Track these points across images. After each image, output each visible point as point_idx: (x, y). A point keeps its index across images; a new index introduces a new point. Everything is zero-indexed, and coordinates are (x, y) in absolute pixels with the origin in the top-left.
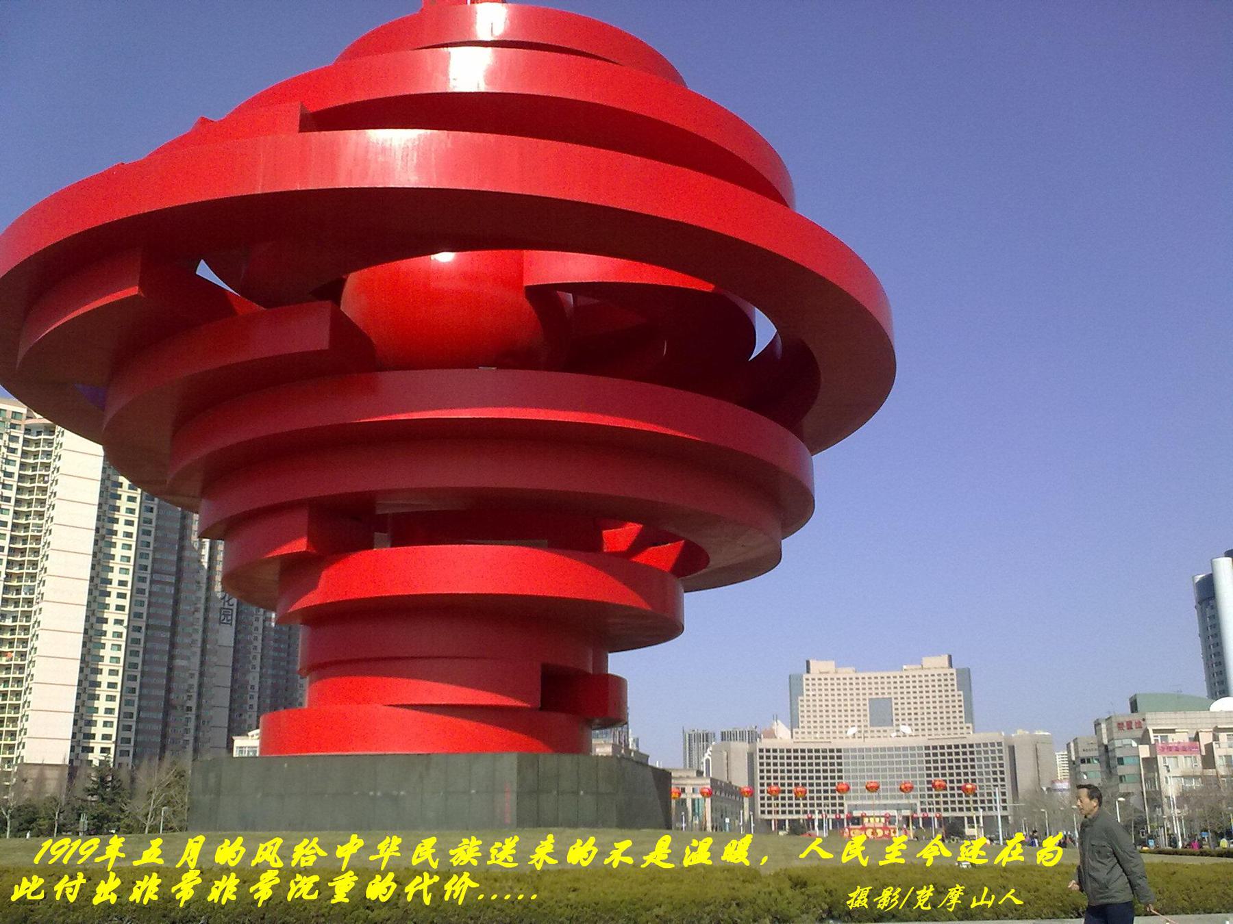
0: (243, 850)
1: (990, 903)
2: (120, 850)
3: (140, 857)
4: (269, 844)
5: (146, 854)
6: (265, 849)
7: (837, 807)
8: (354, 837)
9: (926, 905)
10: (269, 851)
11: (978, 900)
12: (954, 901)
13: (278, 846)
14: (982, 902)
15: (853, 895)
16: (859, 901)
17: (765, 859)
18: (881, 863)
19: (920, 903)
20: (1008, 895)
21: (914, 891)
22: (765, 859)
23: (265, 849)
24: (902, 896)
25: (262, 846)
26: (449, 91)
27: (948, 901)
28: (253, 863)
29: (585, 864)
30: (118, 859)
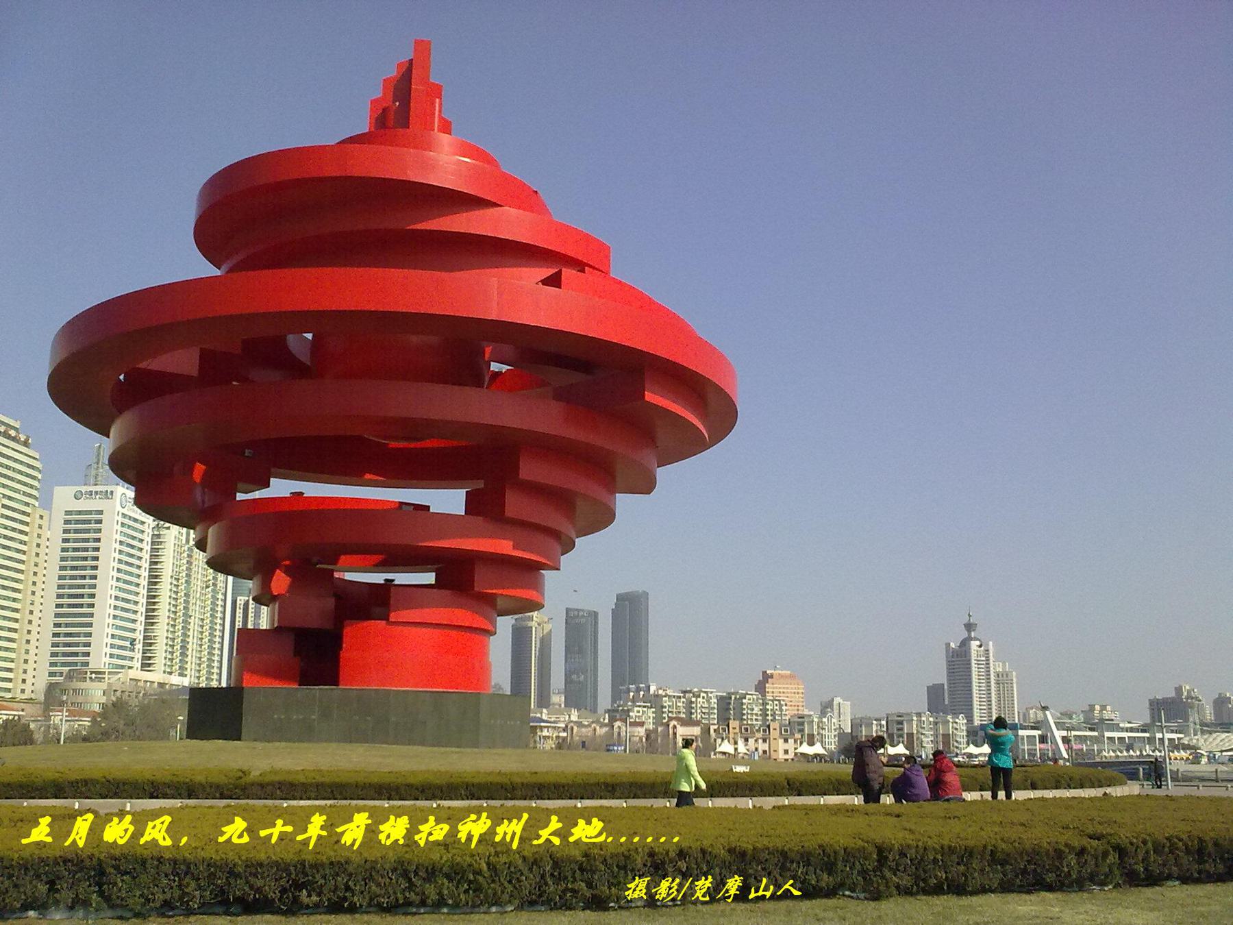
0: (132, 828)
1: (768, 894)
2: (322, 828)
3: (28, 836)
4: (158, 822)
5: (35, 832)
6: (154, 827)
7: (974, 776)
8: (238, 819)
9: (704, 896)
10: (157, 829)
11: (757, 891)
12: (732, 892)
13: (166, 824)
14: (760, 893)
15: (632, 886)
16: (637, 892)
17: (184, 840)
18: (24, 841)
19: (699, 894)
20: (787, 886)
21: (692, 882)
22: (184, 840)
23: (154, 827)
24: (681, 886)
25: (150, 824)
26: (357, 173)
27: (727, 891)
28: (142, 841)
29: (121, 842)
30: (320, 837)
